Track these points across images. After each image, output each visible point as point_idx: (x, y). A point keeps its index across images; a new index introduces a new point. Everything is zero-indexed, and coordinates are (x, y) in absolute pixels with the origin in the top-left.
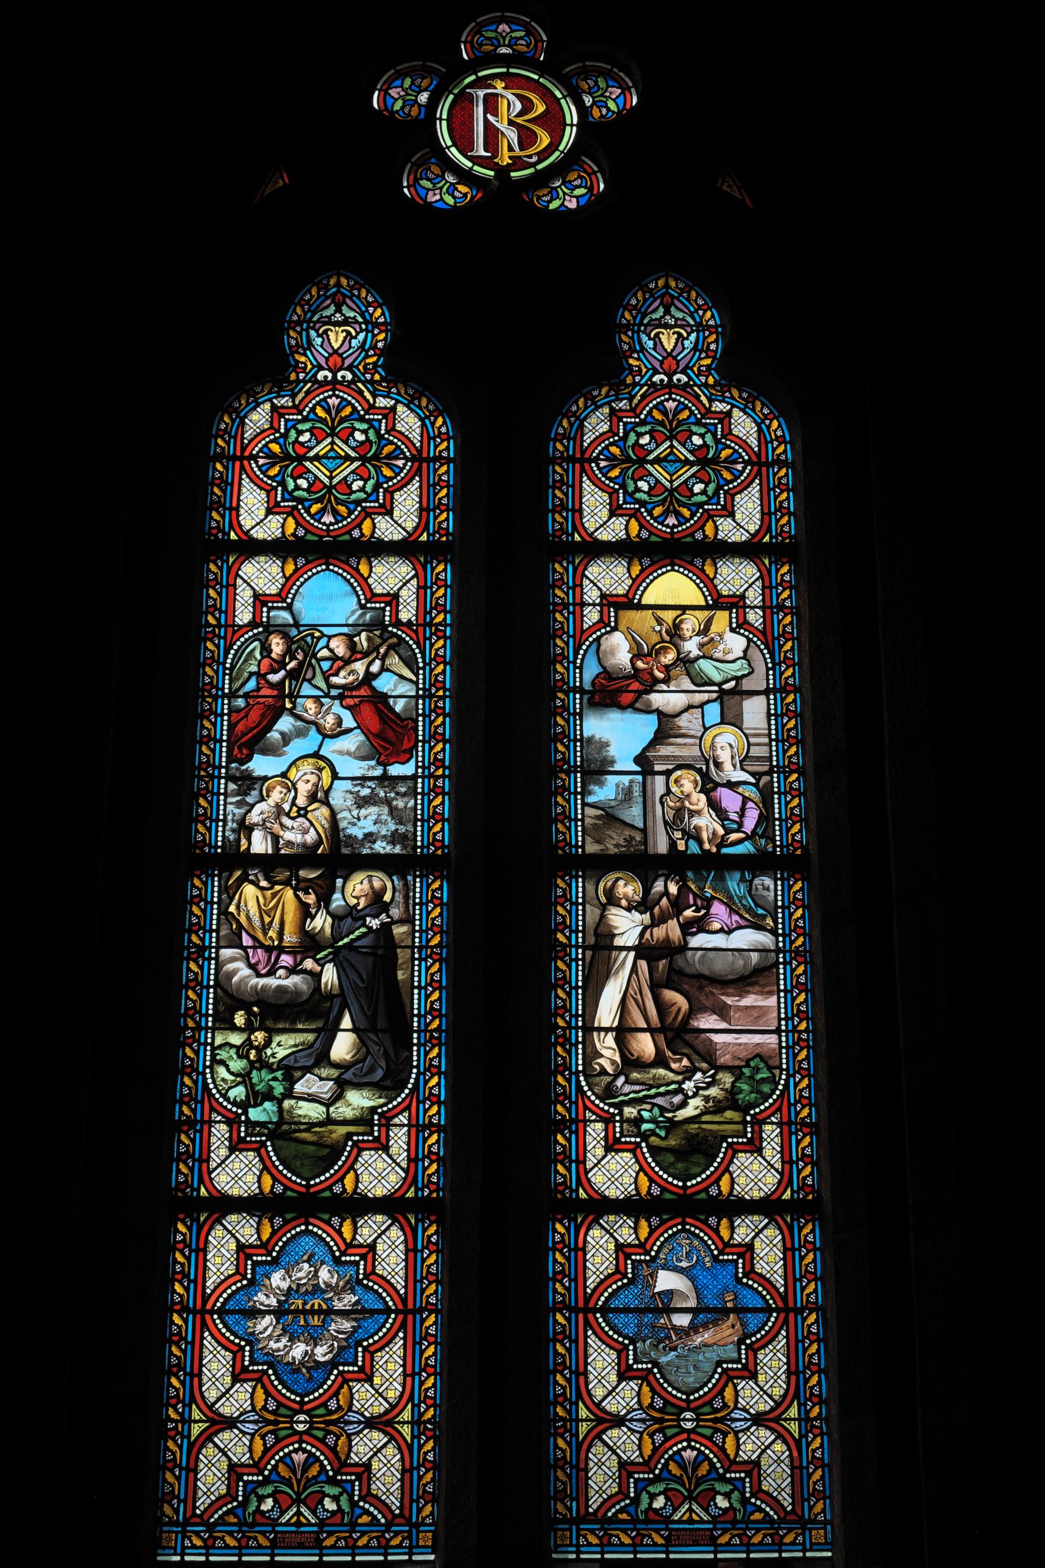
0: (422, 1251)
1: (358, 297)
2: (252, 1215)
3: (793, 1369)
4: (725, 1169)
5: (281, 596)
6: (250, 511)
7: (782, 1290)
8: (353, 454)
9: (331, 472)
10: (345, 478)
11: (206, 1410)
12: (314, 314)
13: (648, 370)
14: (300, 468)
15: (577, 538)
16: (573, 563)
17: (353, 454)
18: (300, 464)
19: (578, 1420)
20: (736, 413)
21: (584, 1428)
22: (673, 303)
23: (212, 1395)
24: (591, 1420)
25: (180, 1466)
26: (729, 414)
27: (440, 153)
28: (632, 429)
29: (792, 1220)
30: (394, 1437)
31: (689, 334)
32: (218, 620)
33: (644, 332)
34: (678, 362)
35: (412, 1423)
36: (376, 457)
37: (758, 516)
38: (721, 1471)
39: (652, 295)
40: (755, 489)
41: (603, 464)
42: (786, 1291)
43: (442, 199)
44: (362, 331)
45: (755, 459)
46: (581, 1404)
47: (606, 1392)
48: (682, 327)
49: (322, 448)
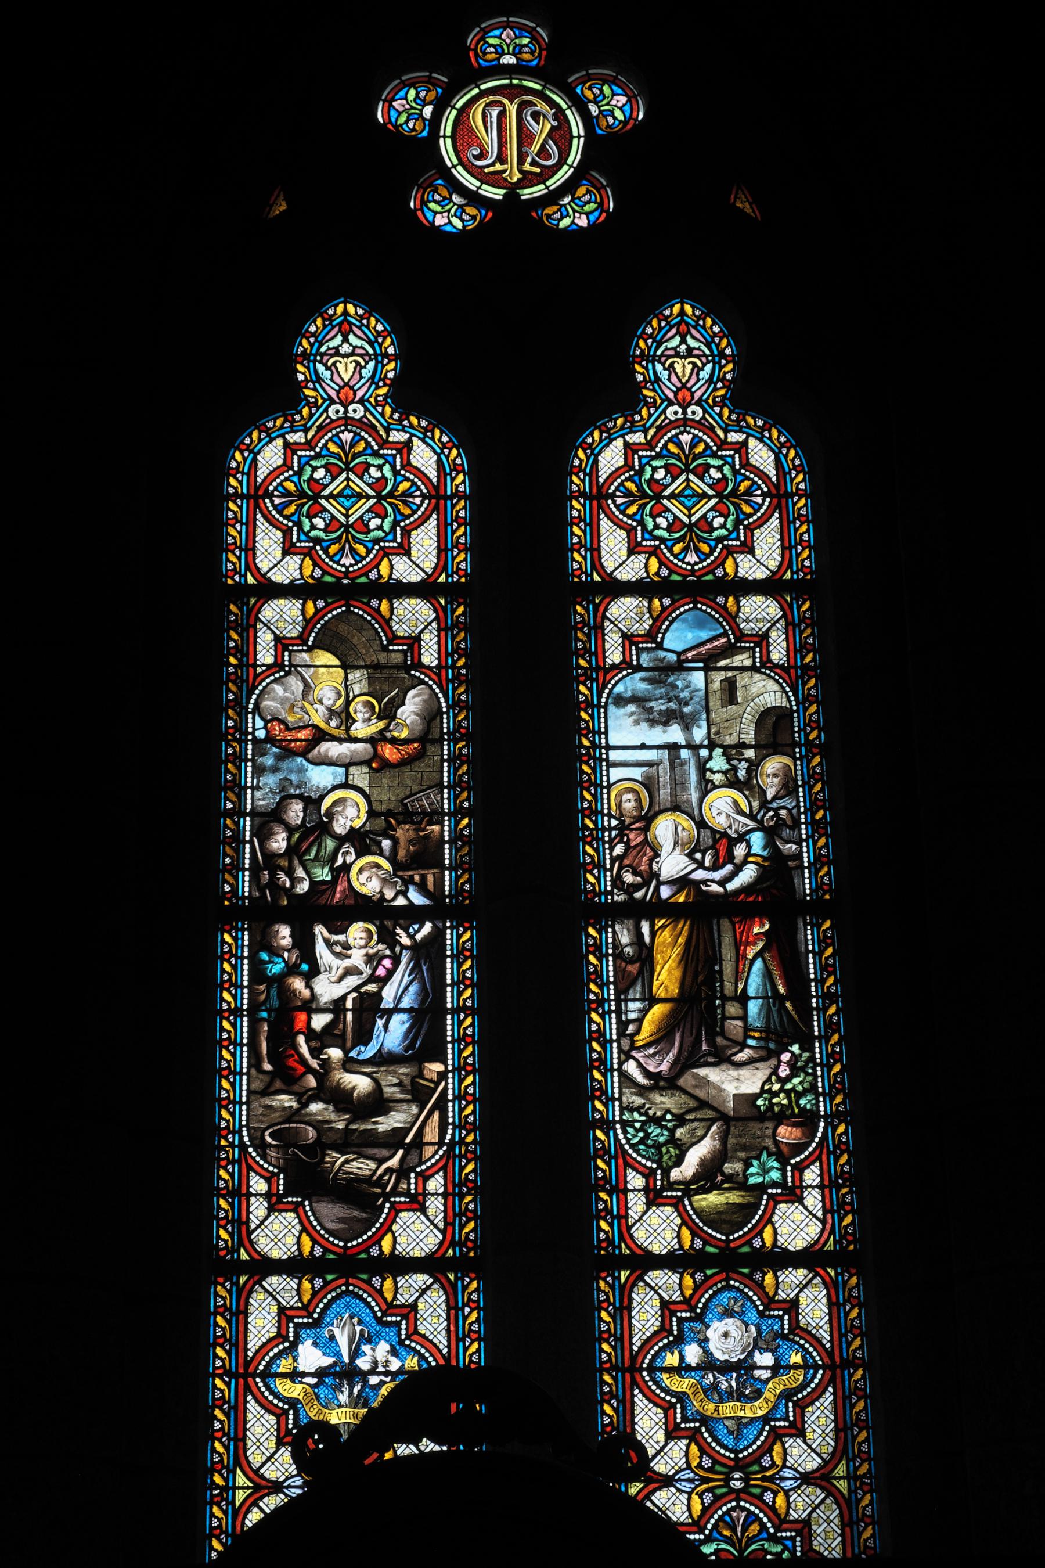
0: (844, 1306)
1: (704, 327)
2: (675, 1271)
3: (841, 1426)
4: (768, 1220)
5: (651, 635)
6: (267, 553)
7: (828, 1345)
8: (711, 492)
9: (347, 510)
10: (361, 517)
11: (251, 1475)
12: (321, 345)
13: (325, 400)
14: (317, 506)
15: (251, 580)
16: (593, 602)
17: (711, 492)
18: (658, 502)
19: (235, 1488)
20: (752, 443)
21: (240, 1496)
22: (689, 332)
23: (256, 1460)
24: (835, 1478)
25: (226, 1532)
26: (745, 444)
27: (446, 173)
28: (307, 463)
29: (456, 1278)
30: (830, 1491)
31: (367, 363)
32: (589, 662)
33: (321, 362)
34: (692, 394)
35: (847, 1477)
36: (734, 492)
37: (435, 553)
38: (772, 1530)
39: (668, 323)
40: (774, 522)
41: (619, 501)
42: (832, 1346)
43: (450, 222)
44: (708, 362)
45: (774, 491)
46: (238, 1471)
47: (264, 1458)
48: (698, 357)
49: (336, 486)
